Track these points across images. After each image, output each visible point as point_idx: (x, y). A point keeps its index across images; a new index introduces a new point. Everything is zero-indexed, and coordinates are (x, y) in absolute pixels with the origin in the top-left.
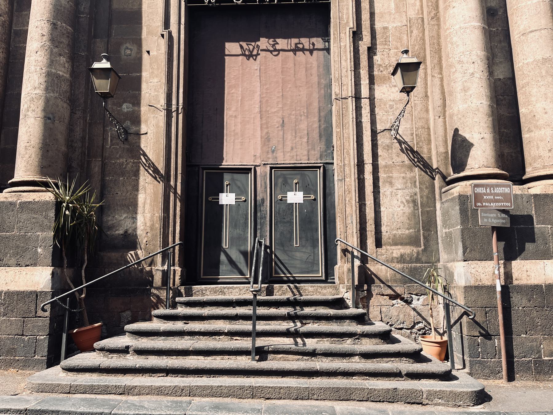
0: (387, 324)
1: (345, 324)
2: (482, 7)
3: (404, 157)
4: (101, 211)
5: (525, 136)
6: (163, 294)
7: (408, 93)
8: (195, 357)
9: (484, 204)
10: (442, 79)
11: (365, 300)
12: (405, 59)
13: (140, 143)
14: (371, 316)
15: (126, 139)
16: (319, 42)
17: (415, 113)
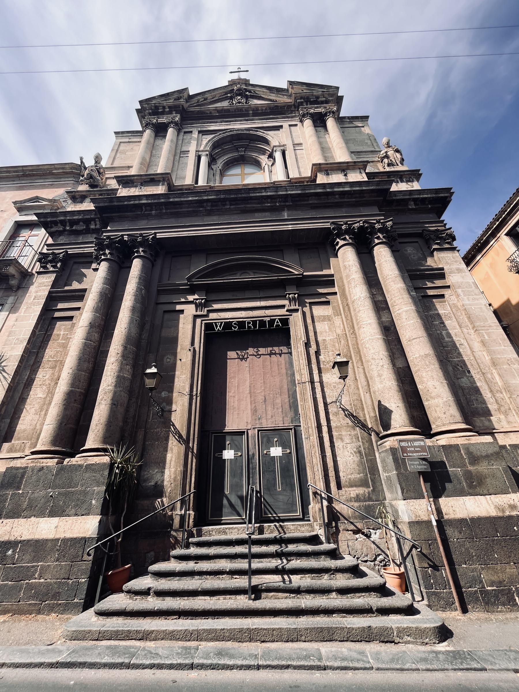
0: (354, 557)
1: (322, 559)
2: (381, 327)
3: (348, 420)
4: (140, 468)
5: (425, 403)
6: (180, 536)
7: (344, 379)
8: (203, 598)
9: (409, 454)
10: (364, 369)
11: (334, 536)
12: (339, 359)
13: (171, 417)
14: (341, 550)
15: (162, 415)
16: (284, 349)
17: (351, 391)
